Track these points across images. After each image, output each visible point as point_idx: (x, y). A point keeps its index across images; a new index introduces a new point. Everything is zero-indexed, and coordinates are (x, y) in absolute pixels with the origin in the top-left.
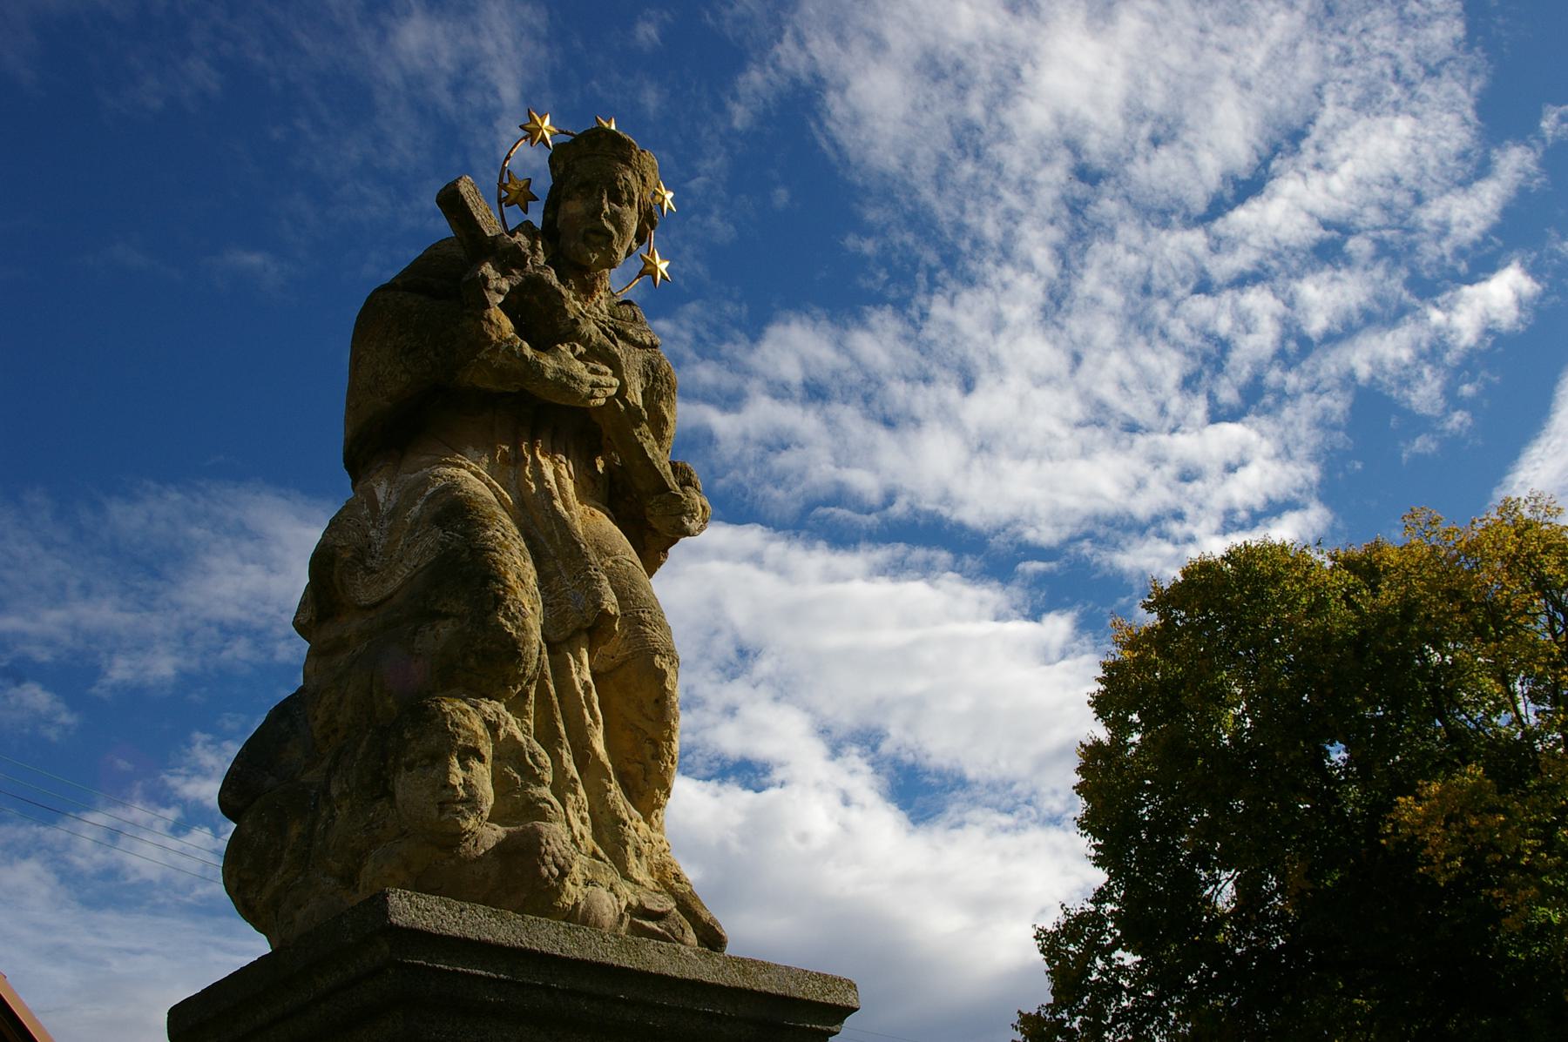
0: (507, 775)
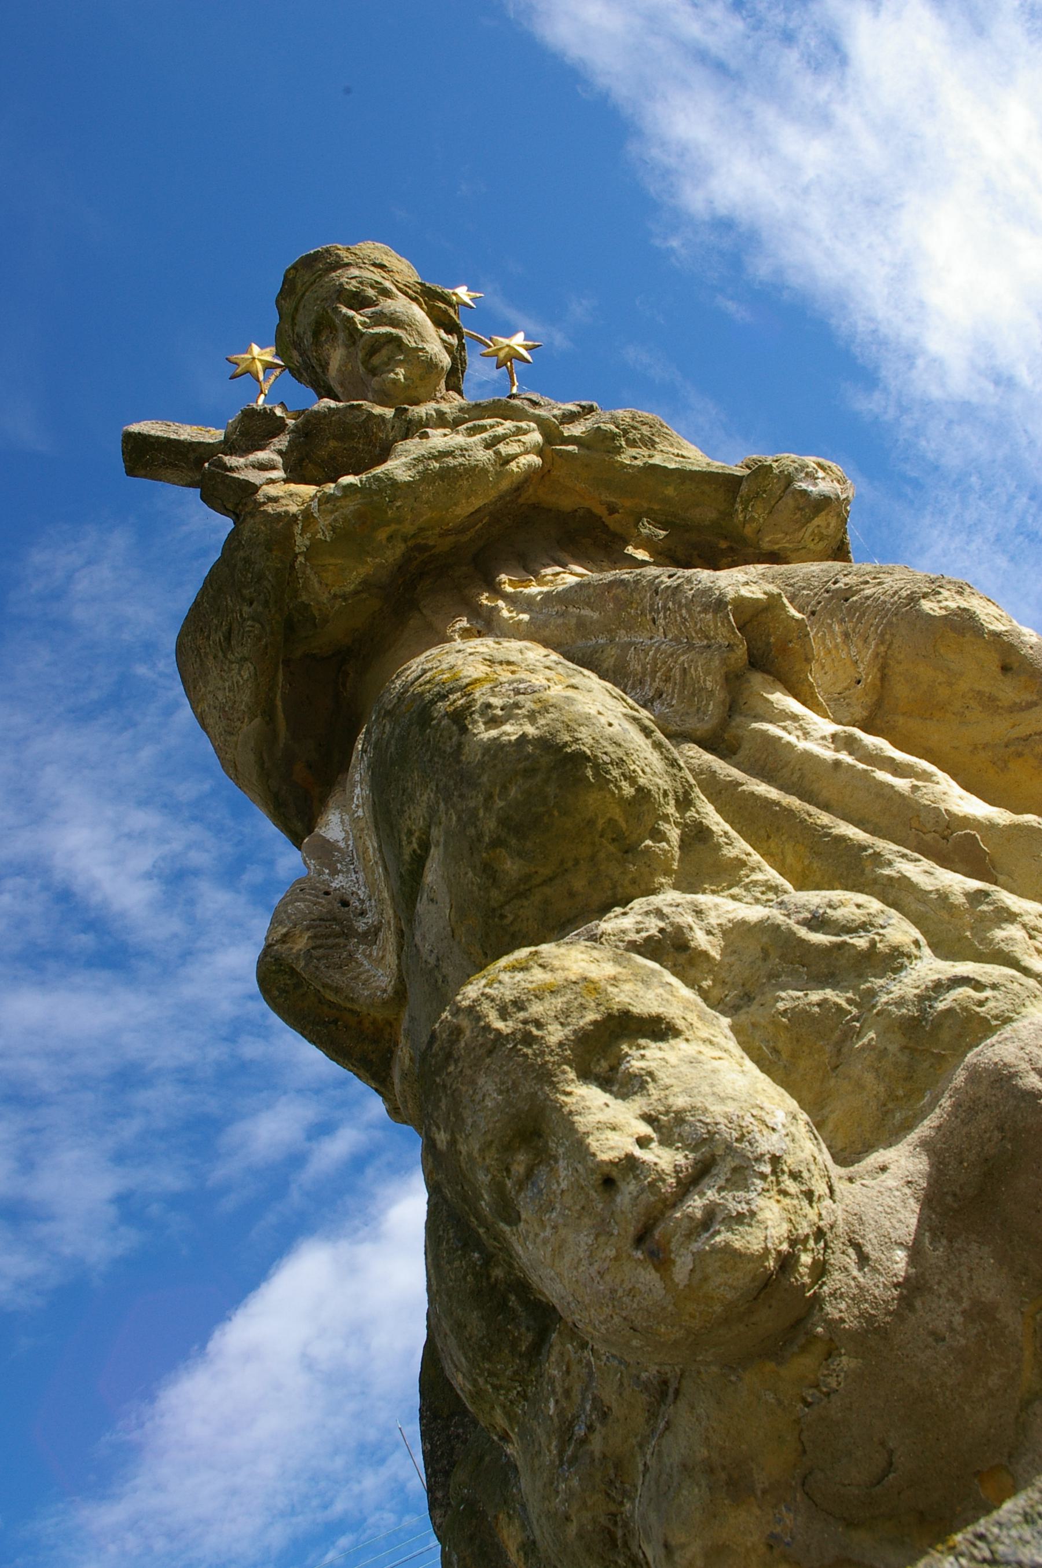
0: (799, 1016)
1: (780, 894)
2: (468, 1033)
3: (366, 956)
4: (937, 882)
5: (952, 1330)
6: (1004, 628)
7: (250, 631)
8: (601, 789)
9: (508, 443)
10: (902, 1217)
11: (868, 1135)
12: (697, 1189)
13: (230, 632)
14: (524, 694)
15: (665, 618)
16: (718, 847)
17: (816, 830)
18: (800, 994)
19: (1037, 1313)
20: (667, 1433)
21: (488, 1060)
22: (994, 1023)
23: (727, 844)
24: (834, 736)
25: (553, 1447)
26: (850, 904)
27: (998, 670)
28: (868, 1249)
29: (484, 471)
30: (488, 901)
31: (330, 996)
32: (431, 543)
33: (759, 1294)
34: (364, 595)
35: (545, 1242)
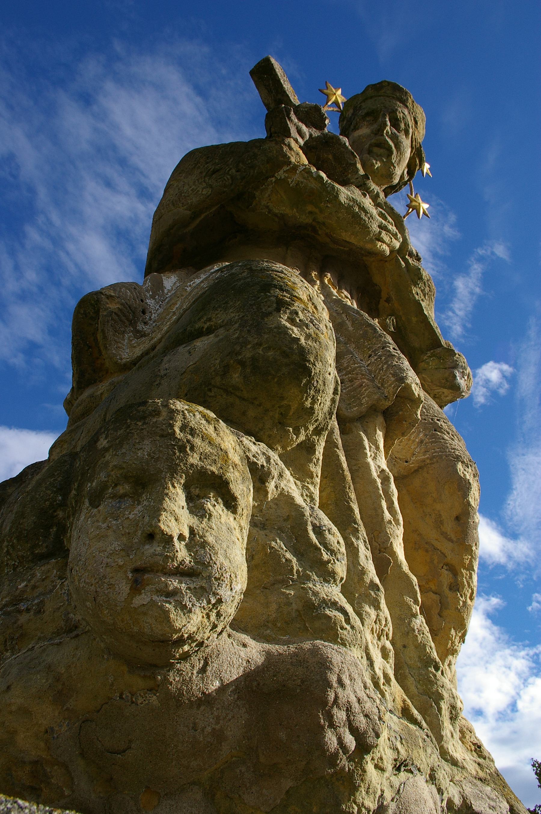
0: (275, 555)
1: (312, 503)
2: (161, 419)
3: (129, 339)
4: (366, 565)
5: (203, 731)
6: (473, 505)
7: (225, 180)
8: (301, 392)
9: (387, 234)
10: (233, 671)
11: (250, 626)
12: (181, 578)
13: (218, 171)
14: (313, 325)
15: (376, 360)
16: (311, 461)
17: (346, 496)
18: (285, 549)
19: (235, 757)
20: (56, 646)
21: (158, 438)
22: (339, 640)
23: (314, 464)
24: (383, 471)
25: (5, 600)
26: (335, 538)
27: (455, 516)
28: (209, 668)
29: (369, 233)
30: (212, 379)
31: (99, 336)
32: (320, 233)
33: (156, 641)
34: (277, 220)
35: (99, 528)
